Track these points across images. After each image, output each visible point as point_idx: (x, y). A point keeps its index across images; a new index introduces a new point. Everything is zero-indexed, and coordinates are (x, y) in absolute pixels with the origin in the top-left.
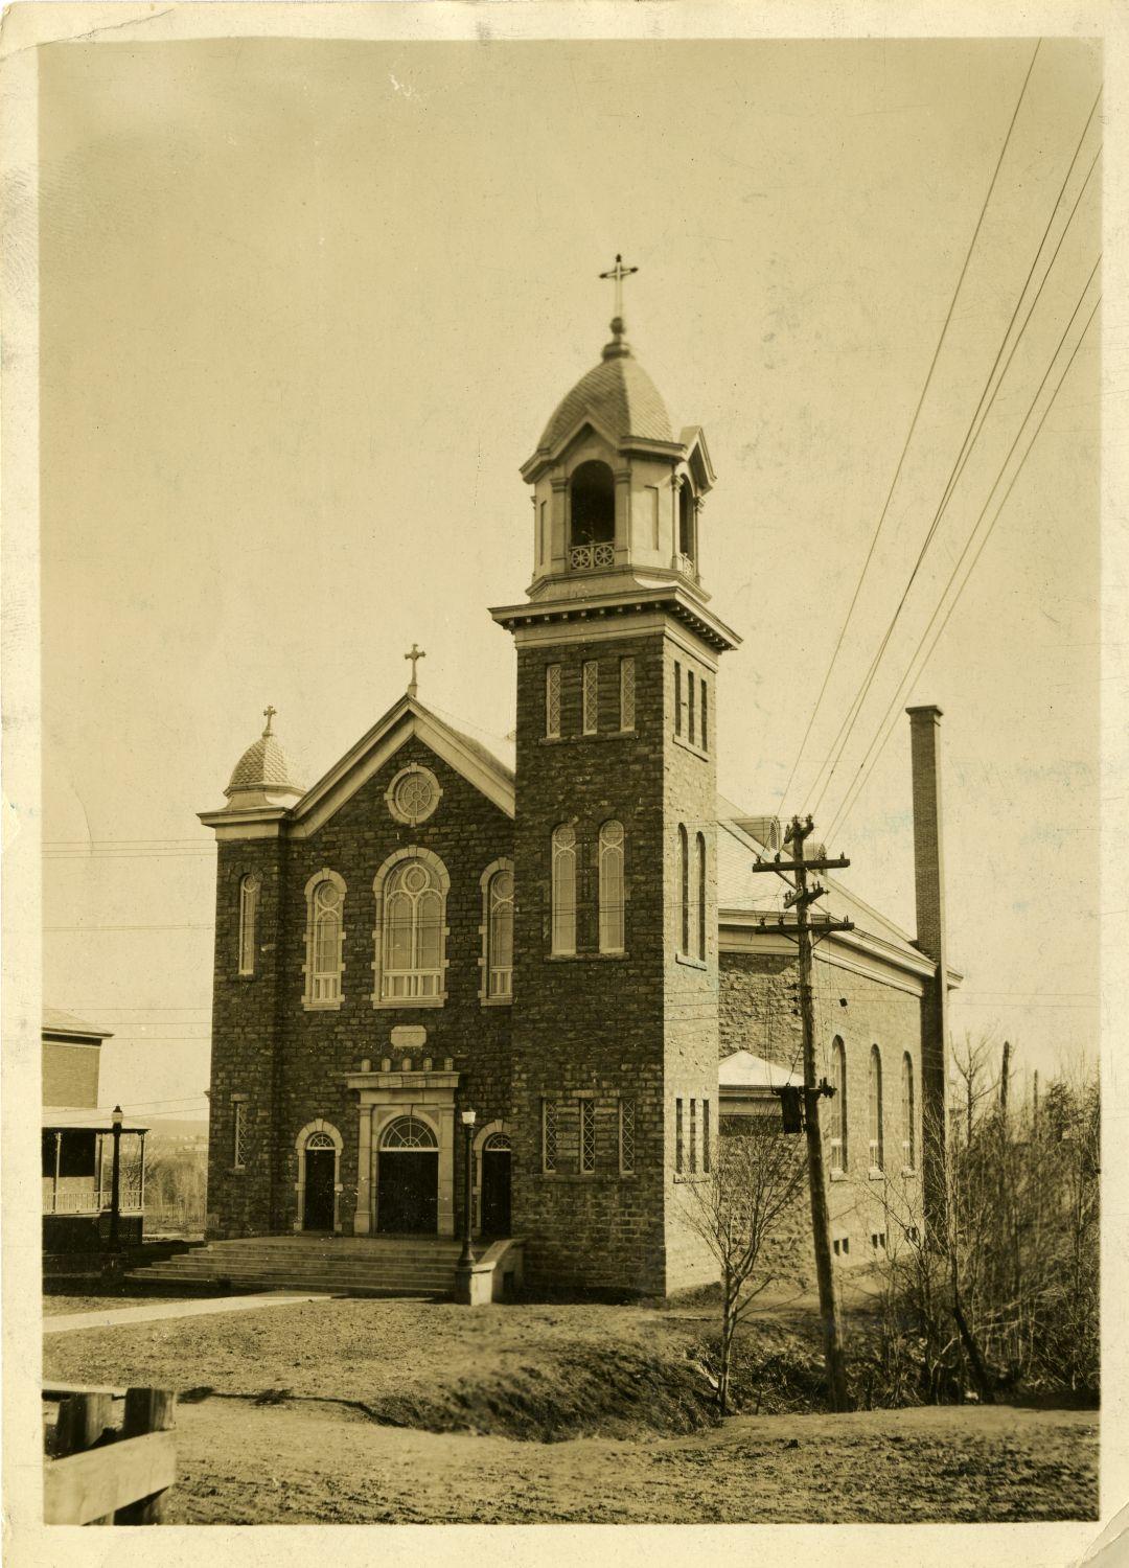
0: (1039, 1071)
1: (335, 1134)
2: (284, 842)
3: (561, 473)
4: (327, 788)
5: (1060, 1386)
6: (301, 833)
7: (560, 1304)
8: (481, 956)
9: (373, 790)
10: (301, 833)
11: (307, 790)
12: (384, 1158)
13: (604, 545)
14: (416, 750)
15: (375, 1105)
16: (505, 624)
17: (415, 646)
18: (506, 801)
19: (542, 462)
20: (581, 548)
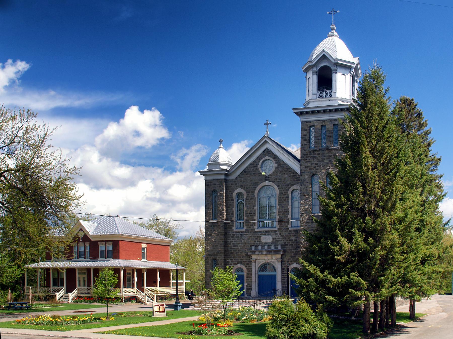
0: (436, 141)
1: (244, 268)
2: (226, 180)
3: (315, 69)
4: (240, 164)
5: (344, 201)
6: (232, 177)
7: (130, 259)
8: (289, 214)
9: (254, 164)
10: (232, 177)
11: (233, 165)
12: (260, 277)
13: (329, 91)
14: (268, 152)
15: (256, 259)
16: (296, 113)
17: (267, 121)
18: (296, 167)
19: (309, 65)
20: (321, 92)
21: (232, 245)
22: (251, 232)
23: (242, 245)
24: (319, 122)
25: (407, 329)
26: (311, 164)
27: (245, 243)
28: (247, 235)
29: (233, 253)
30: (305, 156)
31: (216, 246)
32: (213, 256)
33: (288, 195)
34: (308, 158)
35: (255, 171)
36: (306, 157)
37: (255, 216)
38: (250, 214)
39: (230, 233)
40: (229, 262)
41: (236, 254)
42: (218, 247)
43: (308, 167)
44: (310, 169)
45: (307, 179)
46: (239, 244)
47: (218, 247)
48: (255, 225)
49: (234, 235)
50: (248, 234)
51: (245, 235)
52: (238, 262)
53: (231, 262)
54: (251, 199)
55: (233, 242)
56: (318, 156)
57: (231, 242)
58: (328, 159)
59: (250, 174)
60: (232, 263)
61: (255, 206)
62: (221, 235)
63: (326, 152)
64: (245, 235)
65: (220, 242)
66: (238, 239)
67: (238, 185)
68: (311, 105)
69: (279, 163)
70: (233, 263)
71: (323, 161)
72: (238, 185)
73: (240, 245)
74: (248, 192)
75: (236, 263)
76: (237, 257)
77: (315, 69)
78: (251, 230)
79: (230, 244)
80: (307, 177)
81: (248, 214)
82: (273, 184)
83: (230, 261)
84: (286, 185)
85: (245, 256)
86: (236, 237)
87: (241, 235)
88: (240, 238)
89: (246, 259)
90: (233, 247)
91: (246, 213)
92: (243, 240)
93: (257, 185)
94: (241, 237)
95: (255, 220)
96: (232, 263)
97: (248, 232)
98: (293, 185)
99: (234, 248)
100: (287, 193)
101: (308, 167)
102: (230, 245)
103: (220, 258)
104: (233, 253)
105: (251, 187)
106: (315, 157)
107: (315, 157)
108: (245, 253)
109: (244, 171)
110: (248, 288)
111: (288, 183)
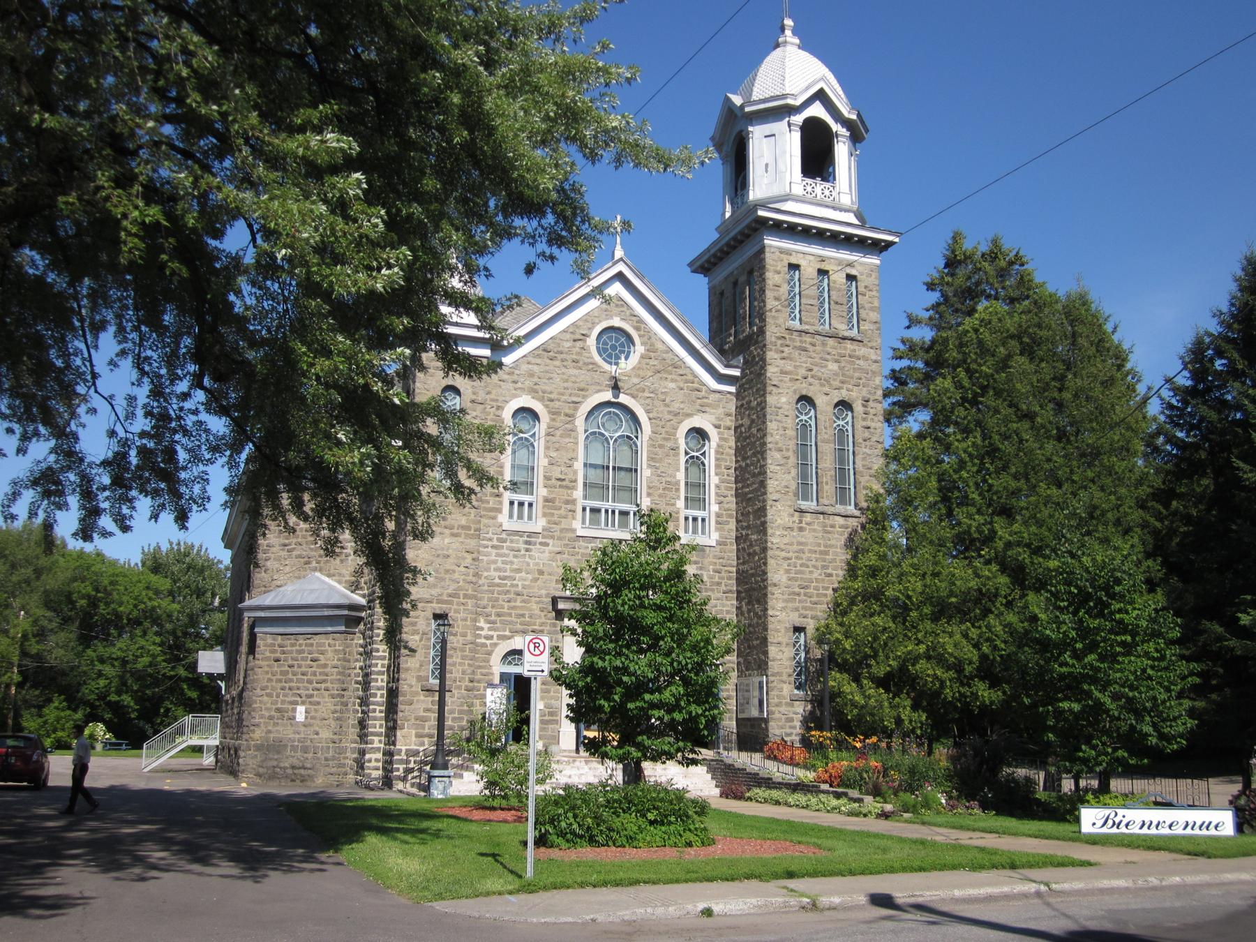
21: (493, 573)
22: (560, 539)
23: (530, 576)
24: (812, 258)
25: (434, 825)
26: (795, 367)
27: (541, 572)
28: (547, 545)
29: (497, 600)
30: (779, 342)
31: (447, 571)
32: (434, 605)
33: (676, 440)
34: (786, 349)
35: (578, 354)
36: (782, 345)
37: (574, 488)
38: (559, 479)
39: (490, 535)
40: (482, 629)
41: (506, 605)
42: (456, 576)
43: (786, 373)
44: (791, 380)
45: (786, 407)
46: (519, 571)
47: (456, 576)
48: (574, 518)
49: (505, 541)
50: (550, 541)
51: (541, 544)
52: (515, 632)
53: (490, 629)
54: (561, 436)
55: (499, 564)
56: (811, 348)
57: (489, 562)
58: (837, 361)
59: (562, 361)
60: (491, 633)
61: (576, 459)
62: (467, 536)
63: (831, 342)
64: (541, 544)
65: (465, 558)
66: (515, 556)
67: (519, 385)
68: (789, 206)
69: (652, 345)
70: (495, 634)
71: (826, 366)
72: (519, 385)
73: (523, 574)
74: (554, 413)
75: (507, 633)
76: (510, 615)
77: (799, 119)
78: (562, 530)
79: (488, 570)
80: (784, 400)
81: (554, 481)
82: (633, 401)
83: (486, 626)
84: (670, 412)
85: (537, 612)
86: (508, 548)
87: (527, 543)
88: (523, 552)
89: (542, 624)
90: (497, 581)
91: (547, 478)
92: (531, 562)
93: (585, 397)
94: (527, 550)
95: (614, 501)
96: (491, 633)
97: (552, 537)
98: (689, 415)
99: (498, 585)
100: (674, 434)
101: (786, 373)
102: (486, 574)
103: (462, 615)
104: (497, 600)
105: (563, 398)
106: (805, 350)
107: (805, 350)
108: (537, 603)
109: (544, 348)
110: (547, 718)
111: (676, 406)
